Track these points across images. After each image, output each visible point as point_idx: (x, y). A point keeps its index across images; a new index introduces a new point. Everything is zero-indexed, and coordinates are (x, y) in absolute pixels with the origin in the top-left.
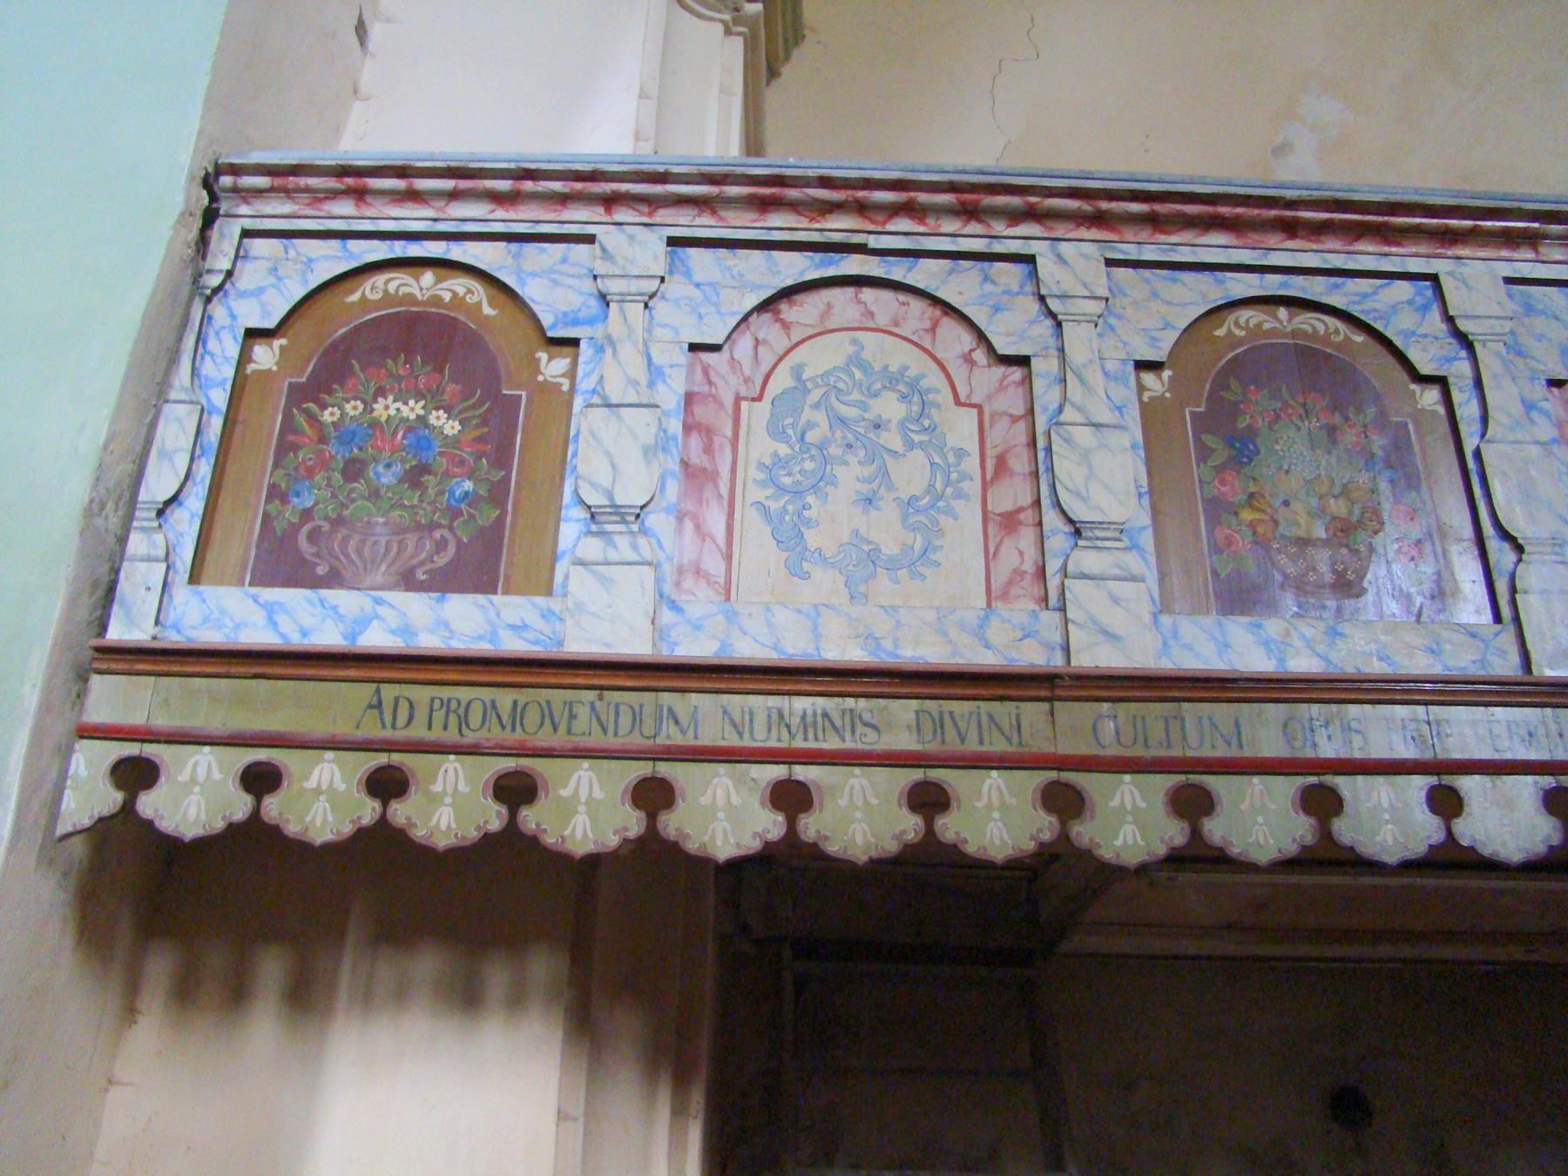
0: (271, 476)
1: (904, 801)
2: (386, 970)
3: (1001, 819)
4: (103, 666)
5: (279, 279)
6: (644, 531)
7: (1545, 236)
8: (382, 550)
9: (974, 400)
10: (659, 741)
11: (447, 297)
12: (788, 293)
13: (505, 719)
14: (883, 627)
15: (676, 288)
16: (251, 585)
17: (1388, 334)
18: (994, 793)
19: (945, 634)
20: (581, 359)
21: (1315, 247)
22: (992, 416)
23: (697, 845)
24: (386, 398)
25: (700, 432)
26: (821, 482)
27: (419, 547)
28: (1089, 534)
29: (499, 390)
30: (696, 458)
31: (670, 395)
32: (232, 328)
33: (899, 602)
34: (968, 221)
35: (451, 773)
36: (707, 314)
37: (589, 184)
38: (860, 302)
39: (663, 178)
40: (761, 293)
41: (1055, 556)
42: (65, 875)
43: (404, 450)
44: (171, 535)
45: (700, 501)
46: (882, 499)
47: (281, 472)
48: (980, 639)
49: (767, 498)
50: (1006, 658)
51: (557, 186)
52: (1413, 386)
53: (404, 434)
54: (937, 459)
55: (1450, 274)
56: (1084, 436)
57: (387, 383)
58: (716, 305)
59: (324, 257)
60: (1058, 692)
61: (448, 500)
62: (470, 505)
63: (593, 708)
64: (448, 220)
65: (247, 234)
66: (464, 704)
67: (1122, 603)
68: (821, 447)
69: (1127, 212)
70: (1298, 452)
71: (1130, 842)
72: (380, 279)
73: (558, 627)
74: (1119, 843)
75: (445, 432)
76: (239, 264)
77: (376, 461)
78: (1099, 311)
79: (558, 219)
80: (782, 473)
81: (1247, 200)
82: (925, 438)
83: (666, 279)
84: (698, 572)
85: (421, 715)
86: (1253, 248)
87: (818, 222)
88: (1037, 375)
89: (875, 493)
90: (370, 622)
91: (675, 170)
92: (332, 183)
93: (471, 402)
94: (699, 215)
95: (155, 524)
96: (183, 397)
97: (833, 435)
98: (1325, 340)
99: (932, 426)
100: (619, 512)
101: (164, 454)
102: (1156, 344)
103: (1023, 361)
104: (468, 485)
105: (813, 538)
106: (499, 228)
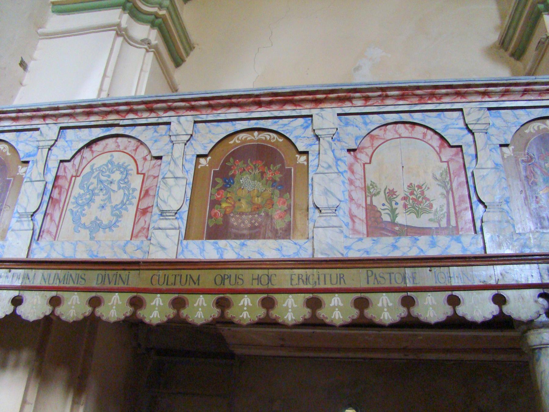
1: (353, 305)
3: (115, 309)
7: (354, 98)
9: (143, 172)
15: (60, 143)
17: (291, 138)
18: (115, 301)
21: (269, 109)
25: (59, 188)
28: (165, 214)
39: (57, 109)
49: (74, 208)
51: (28, 114)
52: (297, 156)
54: (126, 192)
55: (317, 114)
56: (171, 182)
58: (71, 147)
60: (141, 267)
67: (170, 237)
68: (93, 191)
70: (248, 182)
71: (199, 317)
74: (151, 317)
81: (241, 96)
82: (125, 185)
86: (246, 112)
87: (105, 118)
91: (61, 106)
94: (70, 119)
98: (269, 142)
102: (206, 148)
105: (83, 220)
106: (14, 128)
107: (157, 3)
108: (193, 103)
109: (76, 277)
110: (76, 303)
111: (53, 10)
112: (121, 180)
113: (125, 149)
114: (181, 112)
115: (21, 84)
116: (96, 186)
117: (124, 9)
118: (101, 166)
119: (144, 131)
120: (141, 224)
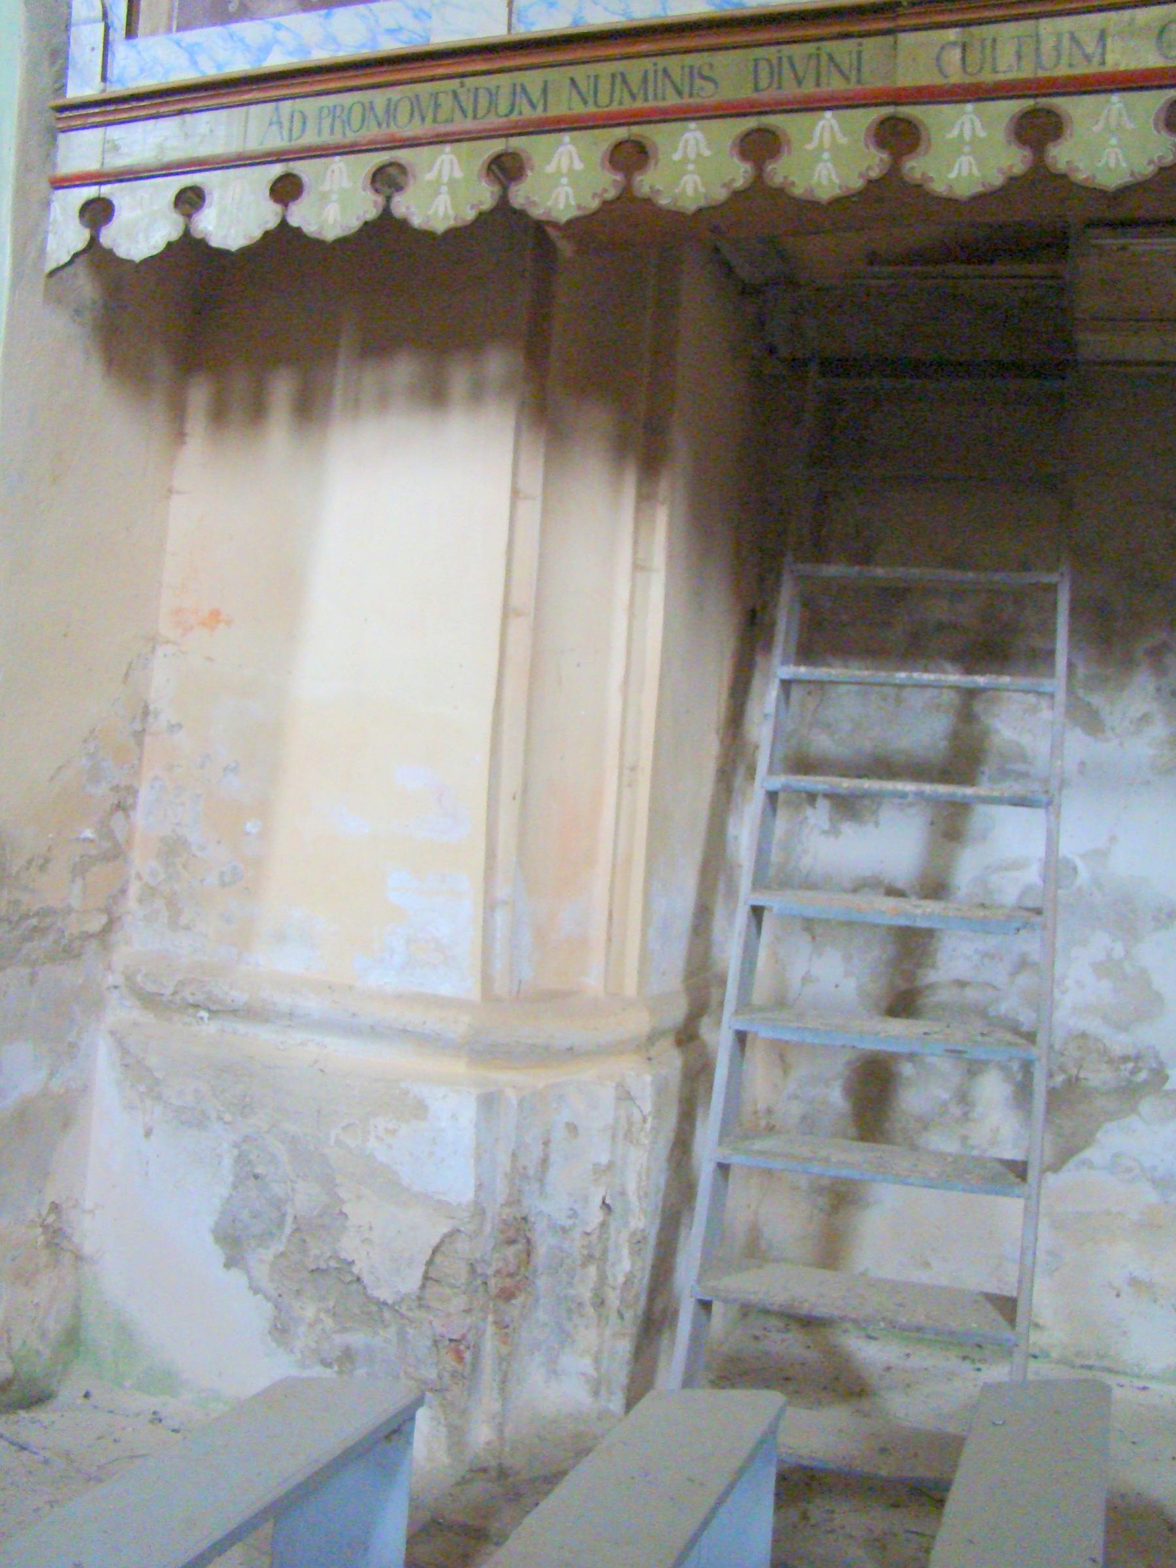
2: (370, 379)
10: (514, 117)
18: (827, 136)
23: (542, 211)
35: (337, 172)
42: (77, 312)
60: (902, 22)
63: (455, 95)
110: (699, 155)
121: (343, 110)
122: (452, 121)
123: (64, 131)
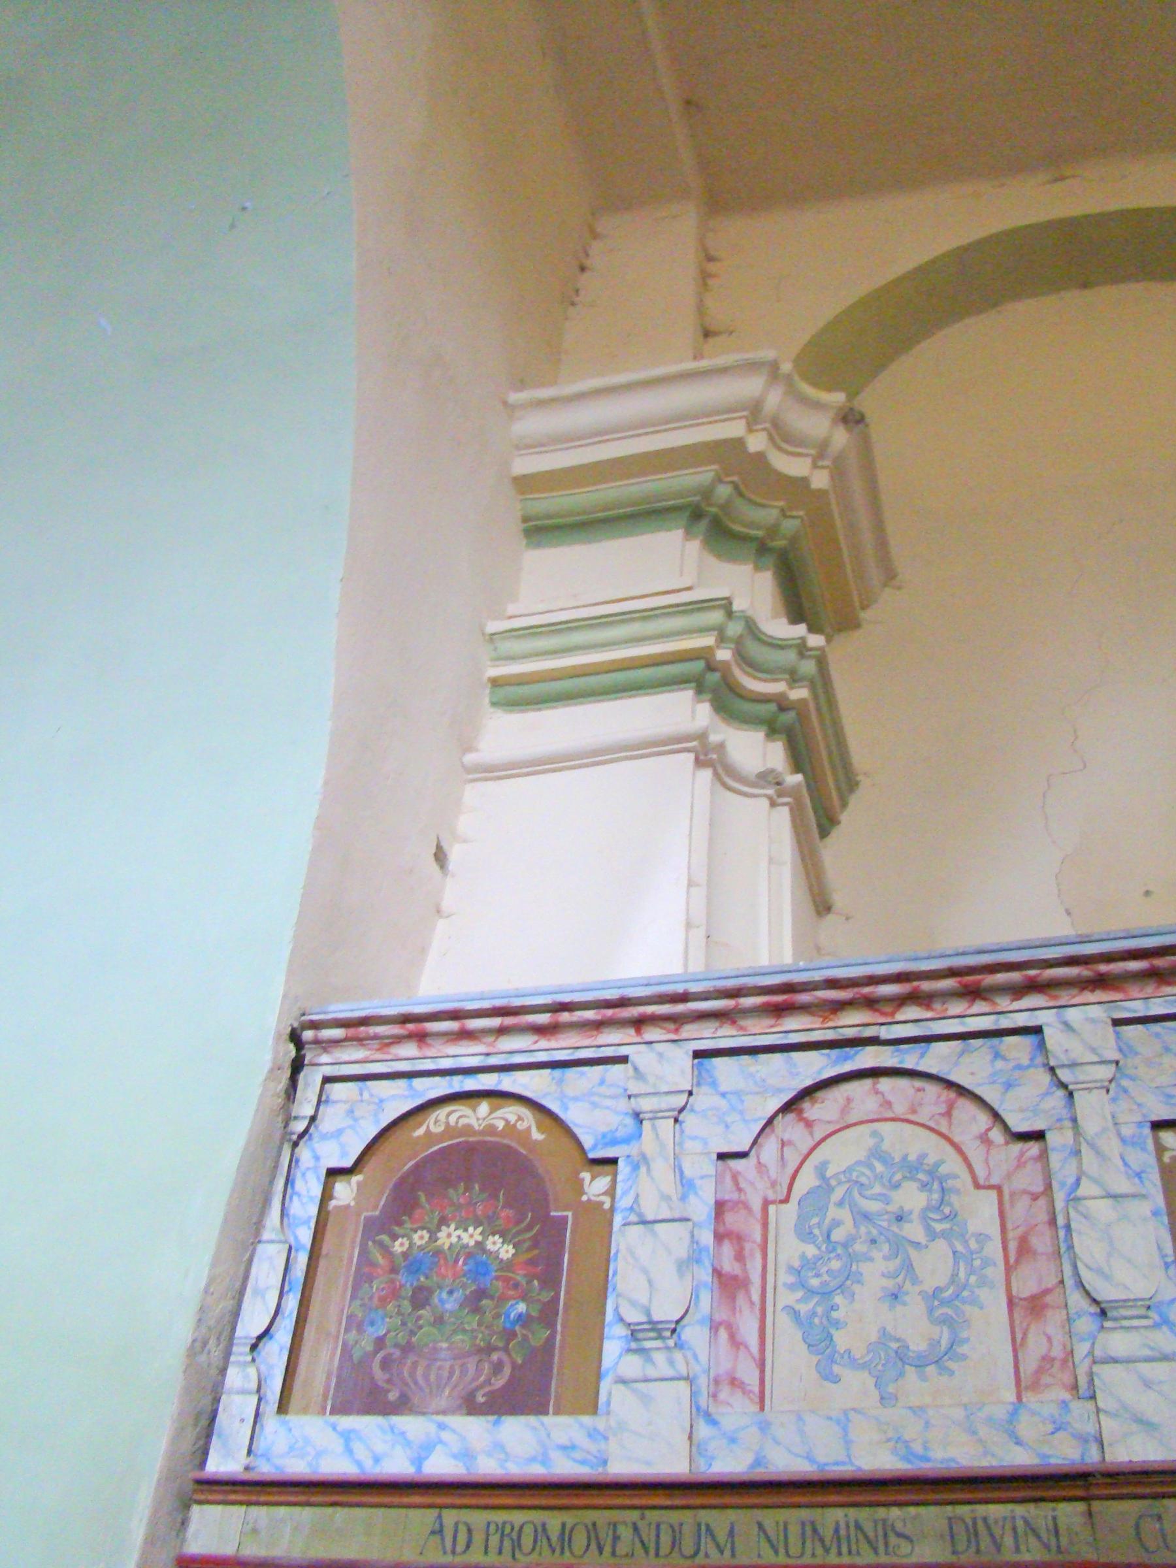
0: (349, 1307)
4: (202, 1497)
5: (356, 1120)
6: (679, 1346)
8: (446, 1374)
9: (995, 1180)
11: (500, 1125)
12: (808, 1093)
13: (554, 1540)
14: (912, 1430)
15: (704, 1099)
16: (331, 1413)
19: (974, 1433)
20: (620, 1178)
22: (1012, 1194)
24: (448, 1226)
26: (847, 1281)
27: (479, 1371)
29: (547, 1215)
30: (729, 1265)
31: (701, 1208)
32: (316, 1169)
33: (928, 1400)
34: (973, 1001)
36: (733, 1122)
37: (617, 1010)
38: (877, 1092)
39: (684, 998)
40: (782, 1096)
41: (1082, 1340)
43: (464, 1275)
44: (263, 1368)
45: (734, 1309)
46: (907, 1294)
47: (358, 1302)
48: (1010, 1436)
49: (798, 1301)
50: (1038, 1455)
51: (590, 1015)
53: (465, 1259)
54: (959, 1247)
56: (1102, 1209)
57: (449, 1212)
58: (741, 1113)
59: (393, 1096)
60: (1095, 1491)
61: (504, 1322)
62: (523, 1326)
63: (636, 1528)
64: (496, 1053)
65: (327, 1080)
66: (516, 1529)
69: (1126, 970)
72: (441, 1113)
73: (603, 1445)
75: (500, 1256)
76: (322, 1108)
77: (440, 1288)
78: (1110, 1076)
79: (596, 1043)
80: (810, 1274)
82: (946, 1225)
83: (694, 1092)
84: (735, 1382)
85: (478, 1539)
87: (831, 1020)
88: (1053, 1149)
89: (900, 1287)
90: (434, 1446)
92: (396, 1030)
93: (523, 1225)
94: (721, 1027)
95: (249, 1358)
96: (273, 1236)
97: (857, 1232)
99: (953, 1214)
100: (654, 1327)
101: (258, 1292)
103: (1039, 1136)
104: (522, 1307)
105: (842, 1339)
107: (783, 670)
108: (1103, 968)
109: (876, 1530)
111: (495, 700)
112: (928, 1208)
113: (914, 1111)
114: (1065, 997)
115: (438, 911)
116: (853, 1231)
117: (700, 690)
118: (849, 1170)
119: (961, 1055)
120: (1035, 1348)
121: (513, 1529)
122: (633, 1555)
123: (200, 1502)
